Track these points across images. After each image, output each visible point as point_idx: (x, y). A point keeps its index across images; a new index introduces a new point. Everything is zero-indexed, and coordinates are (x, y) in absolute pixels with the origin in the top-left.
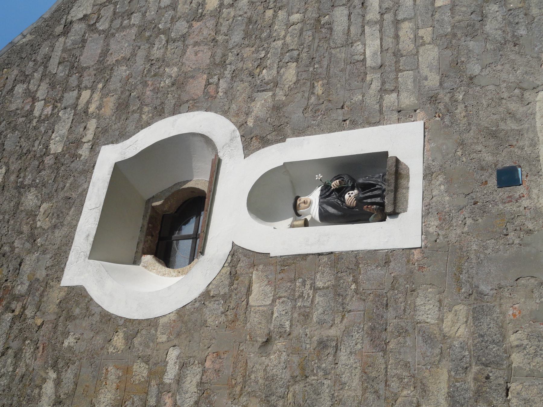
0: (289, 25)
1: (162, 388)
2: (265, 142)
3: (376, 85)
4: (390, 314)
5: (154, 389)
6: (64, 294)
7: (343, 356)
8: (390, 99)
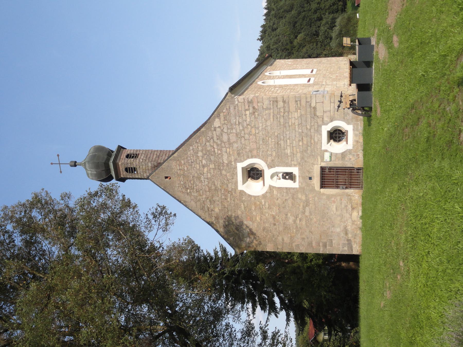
0: (272, 142)
1: (262, 205)
2: (272, 167)
3: (290, 159)
4: (295, 196)
5: (261, 206)
6: (236, 307)
7: (289, 201)
8: (293, 162)
